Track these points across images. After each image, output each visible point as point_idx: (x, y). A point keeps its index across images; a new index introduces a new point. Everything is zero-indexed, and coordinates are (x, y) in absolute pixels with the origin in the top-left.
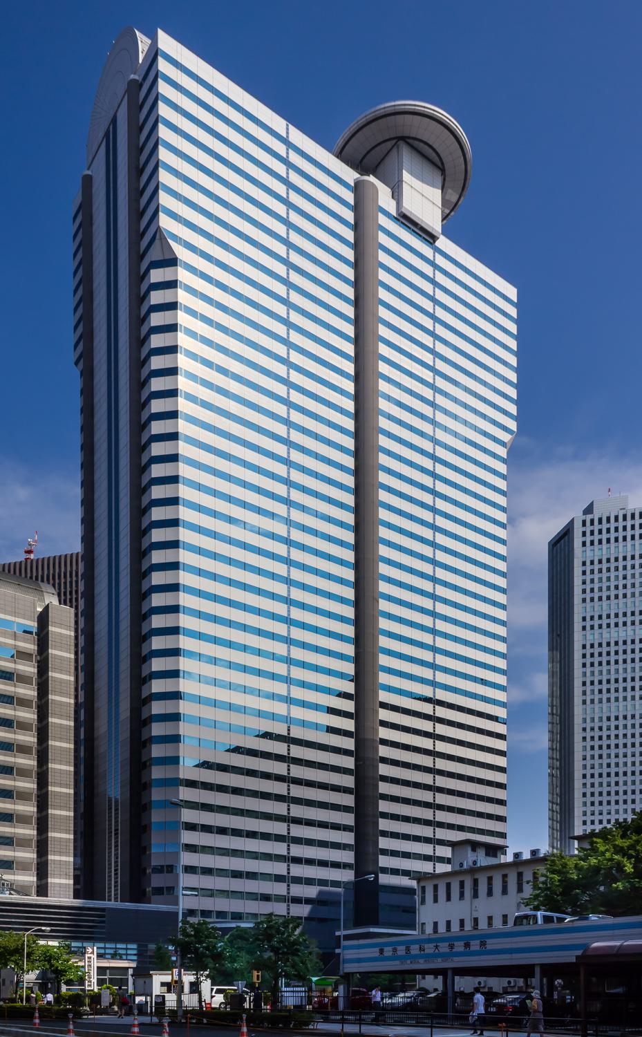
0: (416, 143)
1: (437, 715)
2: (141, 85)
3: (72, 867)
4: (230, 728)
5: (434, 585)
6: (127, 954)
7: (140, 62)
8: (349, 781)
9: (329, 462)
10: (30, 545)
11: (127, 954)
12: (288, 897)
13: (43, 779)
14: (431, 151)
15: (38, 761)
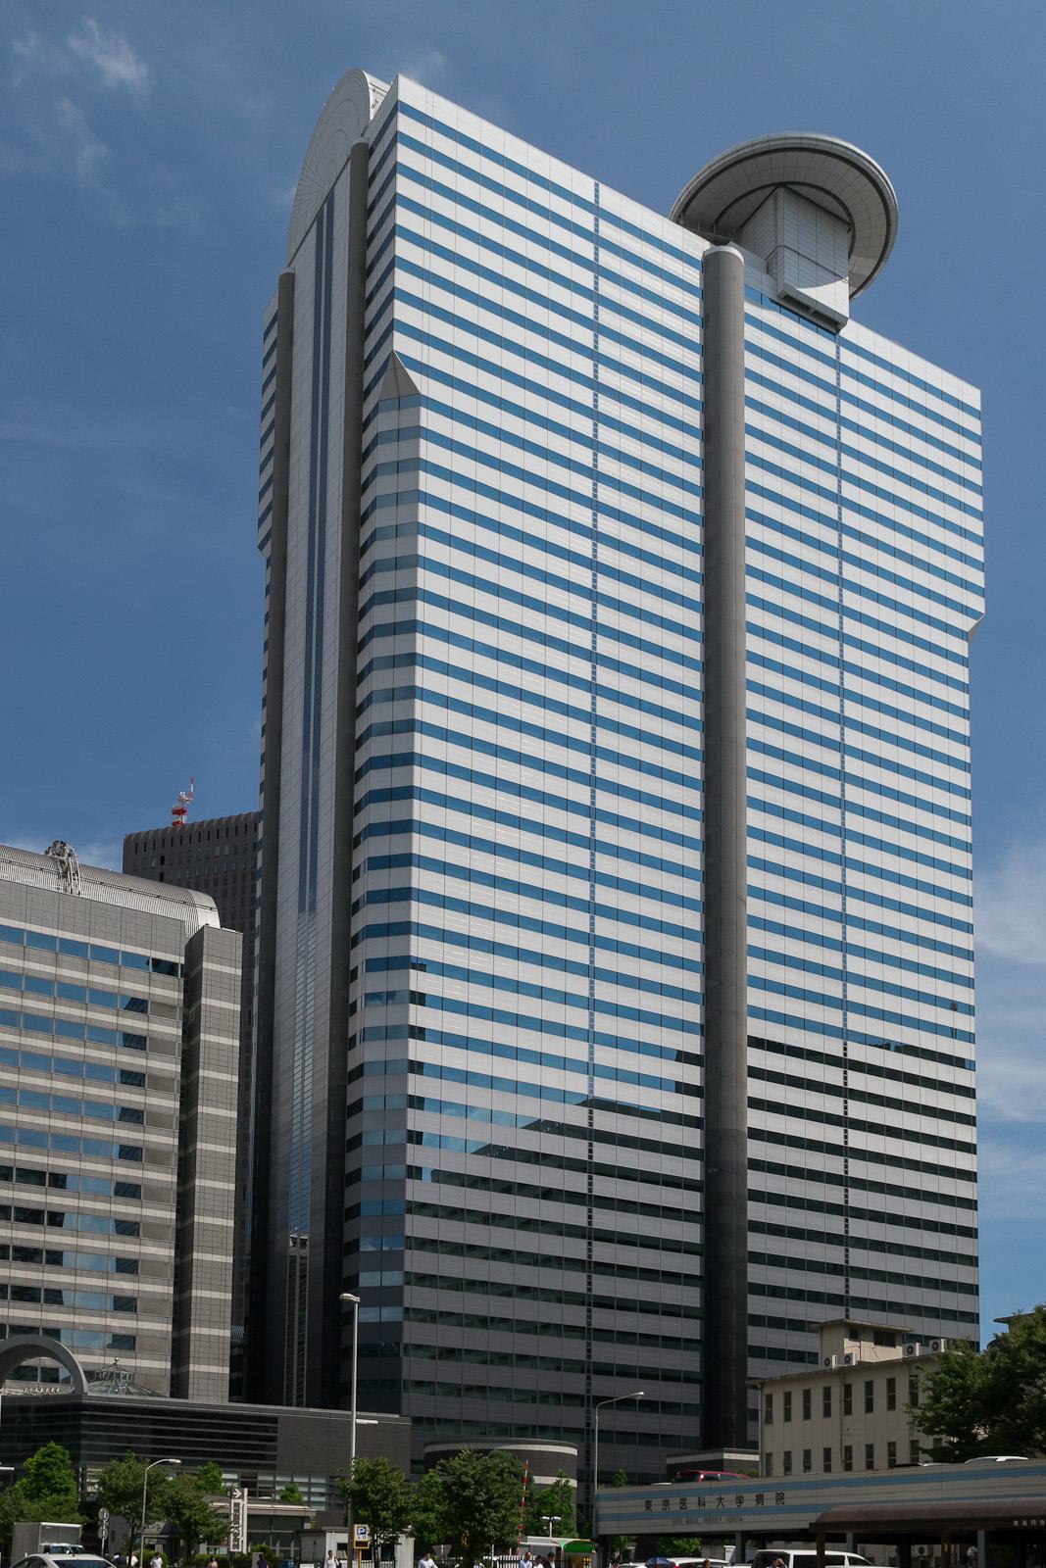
0: (804, 190)
1: (851, 1056)
2: (371, 151)
3: (228, 1346)
4: (492, 1117)
5: (842, 701)
6: (309, 1494)
7: (372, 118)
8: (692, 1170)
9: (661, 865)
10: (182, 800)
11: (309, 1494)
12: (588, 1406)
13: (187, 1132)
14: (829, 198)
15: (179, 1138)
